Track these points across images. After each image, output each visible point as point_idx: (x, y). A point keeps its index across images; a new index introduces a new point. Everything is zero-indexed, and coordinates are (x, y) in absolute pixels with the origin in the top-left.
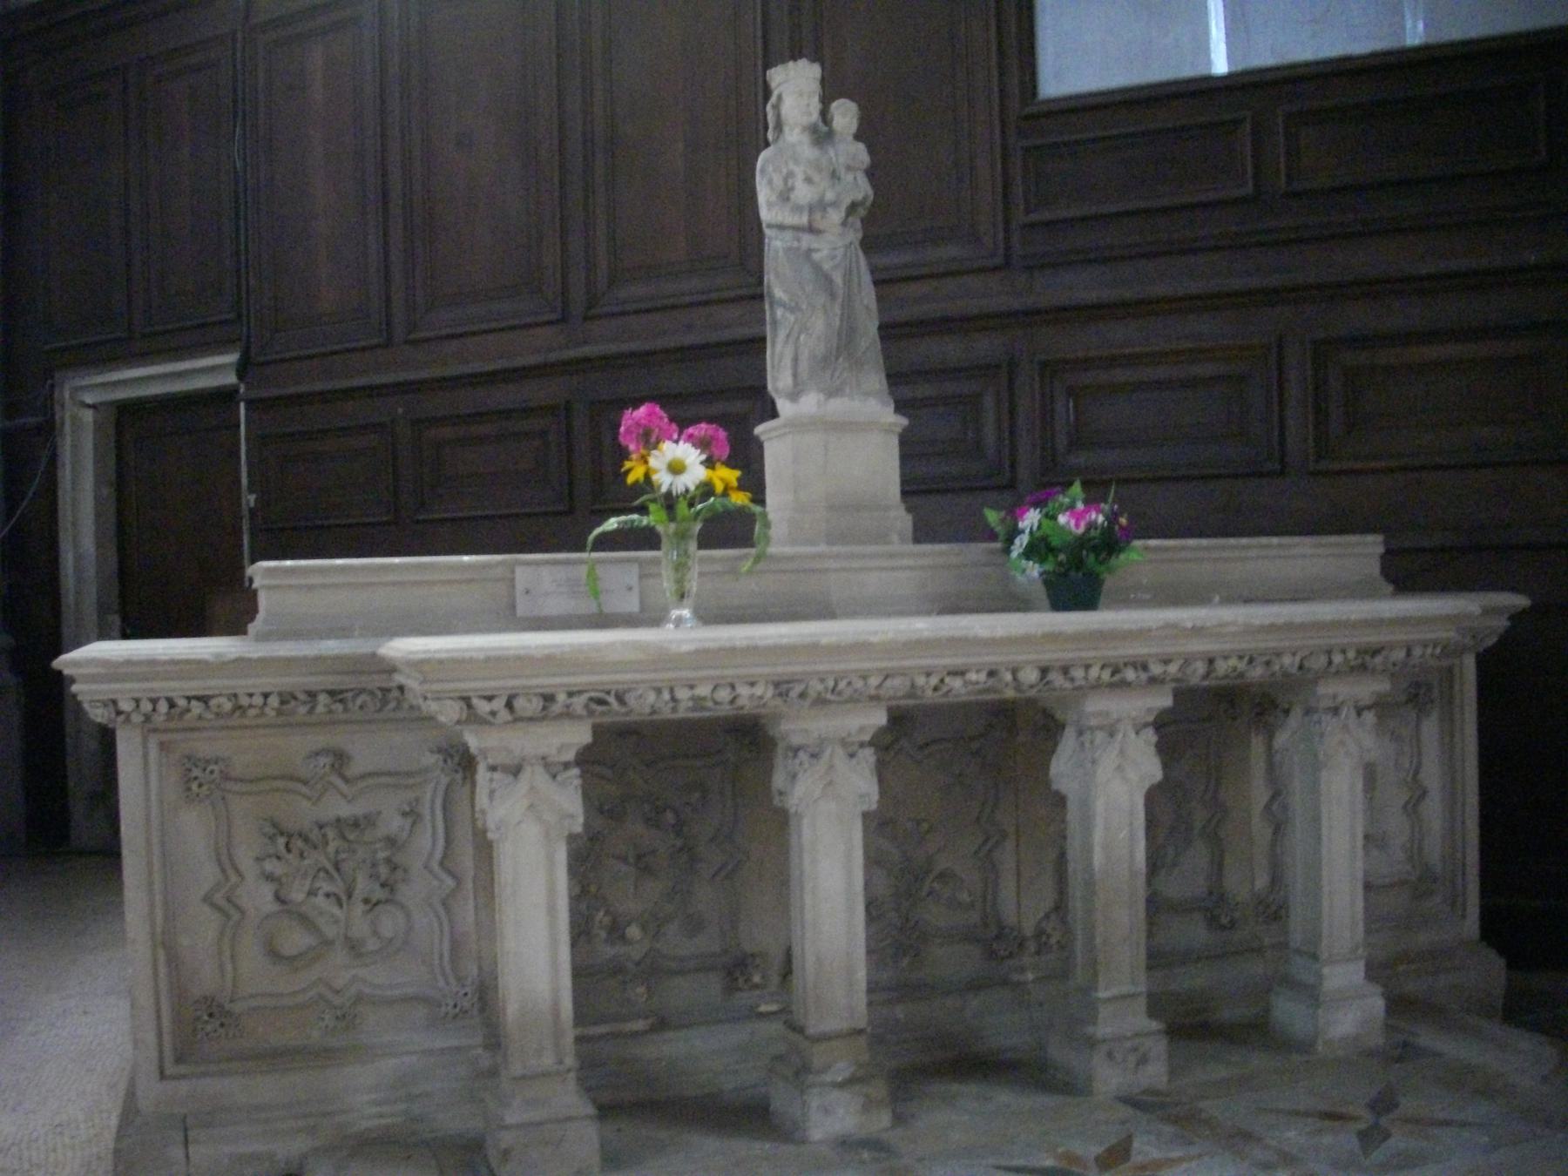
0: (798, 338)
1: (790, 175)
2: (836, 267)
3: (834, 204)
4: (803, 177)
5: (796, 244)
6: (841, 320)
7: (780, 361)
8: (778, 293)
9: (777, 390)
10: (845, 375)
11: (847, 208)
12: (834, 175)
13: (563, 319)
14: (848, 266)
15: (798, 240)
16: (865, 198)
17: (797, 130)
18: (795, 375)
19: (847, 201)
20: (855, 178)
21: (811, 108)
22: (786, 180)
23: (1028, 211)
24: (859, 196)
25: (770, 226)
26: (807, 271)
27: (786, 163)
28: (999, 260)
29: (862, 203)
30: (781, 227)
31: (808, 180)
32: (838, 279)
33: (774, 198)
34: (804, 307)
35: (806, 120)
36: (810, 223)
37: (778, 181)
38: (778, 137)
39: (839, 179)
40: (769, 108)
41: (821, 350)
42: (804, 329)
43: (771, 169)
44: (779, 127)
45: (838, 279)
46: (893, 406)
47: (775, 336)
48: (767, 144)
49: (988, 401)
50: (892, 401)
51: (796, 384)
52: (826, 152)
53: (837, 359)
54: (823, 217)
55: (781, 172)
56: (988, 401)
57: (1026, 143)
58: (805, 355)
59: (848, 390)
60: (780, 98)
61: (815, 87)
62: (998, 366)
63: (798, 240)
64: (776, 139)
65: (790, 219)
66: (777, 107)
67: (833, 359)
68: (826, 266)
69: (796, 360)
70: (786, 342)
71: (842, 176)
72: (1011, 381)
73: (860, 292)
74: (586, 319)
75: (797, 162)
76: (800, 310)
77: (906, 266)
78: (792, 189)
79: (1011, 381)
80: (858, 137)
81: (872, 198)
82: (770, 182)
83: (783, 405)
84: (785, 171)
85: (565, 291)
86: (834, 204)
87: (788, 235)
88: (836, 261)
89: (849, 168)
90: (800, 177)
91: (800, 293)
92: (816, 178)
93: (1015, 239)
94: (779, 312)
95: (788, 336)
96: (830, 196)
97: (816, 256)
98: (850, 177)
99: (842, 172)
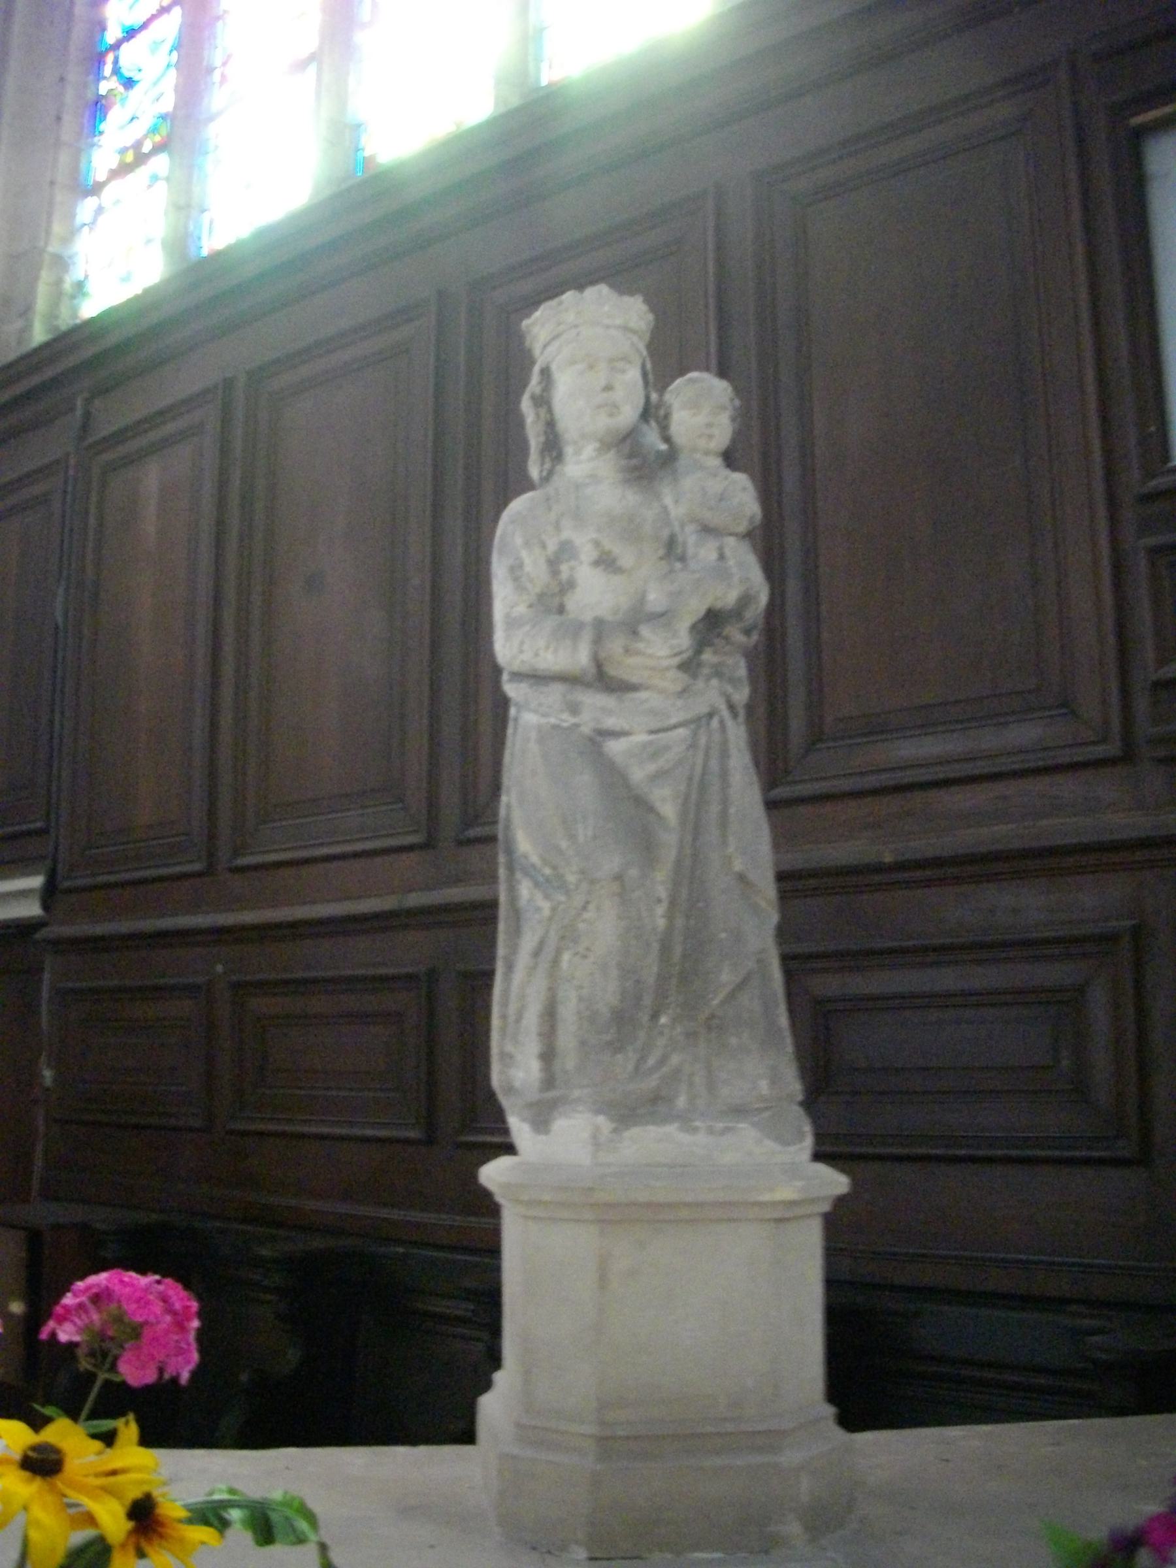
0: (556, 962)
1: (566, 550)
2: (658, 776)
3: (663, 618)
4: (595, 555)
5: (568, 720)
6: (670, 916)
7: (518, 1020)
8: (524, 844)
9: (510, 1090)
10: (675, 1059)
11: (693, 627)
12: (672, 550)
13: (428, 845)
14: (698, 769)
15: (574, 709)
16: (745, 600)
17: (589, 450)
18: (548, 1056)
19: (695, 608)
20: (722, 557)
21: (619, 394)
22: (554, 563)
23: (1162, 662)
24: (729, 597)
25: (517, 676)
26: (585, 780)
27: (557, 527)
28: (1112, 749)
29: (737, 613)
30: (538, 678)
31: (606, 562)
32: (667, 806)
33: (521, 609)
34: (571, 878)
35: (602, 423)
36: (599, 665)
37: (534, 564)
38: (551, 473)
39: (682, 559)
40: (526, 405)
41: (609, 994)
42: (569, 936)
43: (519, 541)
44: (553, 447)
45: (667, 806)
46: (808, 1142)
47: (514, 948)
48: (527, 485)
49: (1098, 999)
50: (808, 1128)
51: (549, 1082)
52: (658, 496)
53: (655, 1016)
54: (627, 651)
55: (544, 546)
56: (1098, 999)
57: (1152, 541)
58: (568, 1011)
59: (681, 1102)
60: (546, 373)
61: (634, 348)
62: (1112, 938)
63: (574, 709)
64: (546, 479)
65: (553, 659)
66: (543, 401)
67: (645, 1018)
68: (638, 774)
69: (550, 1014)
70: (532, 969)
71: (690, 551)
72: (1138, 965)
73: (724, 842)
74: (460, 843)
75: (579, 518)
76: (563, 887)
77: (942, 762)
78: (569, 585)
79: (1138, 965)
80: (730, 459)
81: (763, 598)
82: (516, 570)
83: (519, 1128)
84: (552, 546)
85: (432, 803)
86: (663, 618)
87: (556, 691)
88: (662, 762)
89: (707, 530)
90: (587, 553)
91: (564, 844)
92: (627, 559)
93: (1142, 704)
94: (525, 889)
95: (536, 953)
96: (656, 598)
97: (615, 748)
98: (707, 553)
99: (690, 537)
